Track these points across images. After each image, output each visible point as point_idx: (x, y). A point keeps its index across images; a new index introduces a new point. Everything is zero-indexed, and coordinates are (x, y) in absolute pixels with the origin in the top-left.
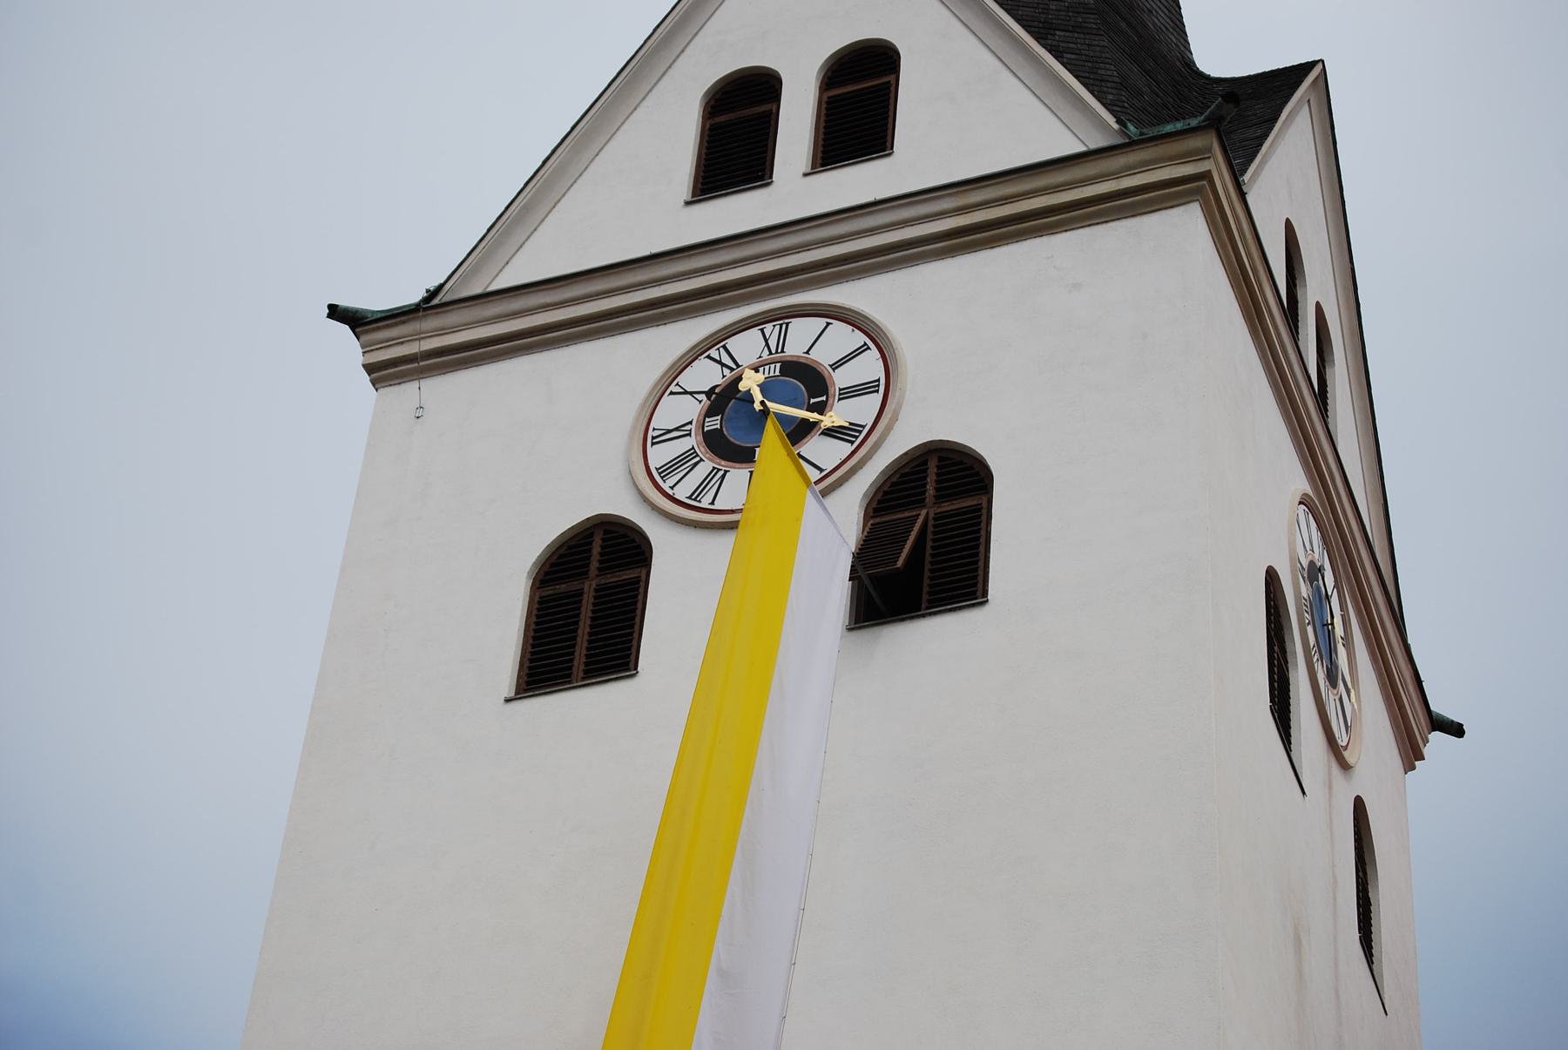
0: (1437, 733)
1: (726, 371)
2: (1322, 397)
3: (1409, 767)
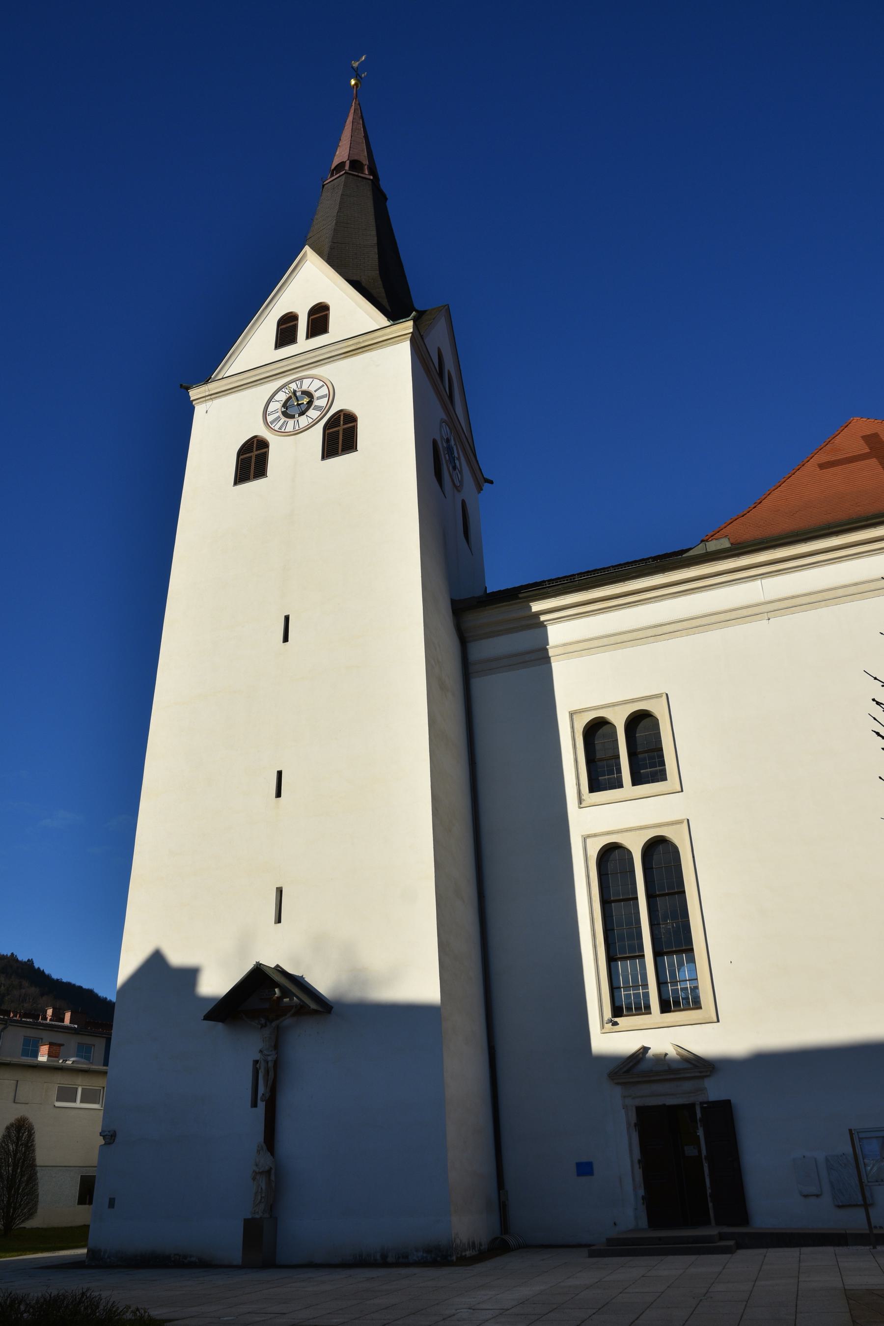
0: (486, 483)
1: (287, 394)
2: (451, 397)
3: (479, 492)
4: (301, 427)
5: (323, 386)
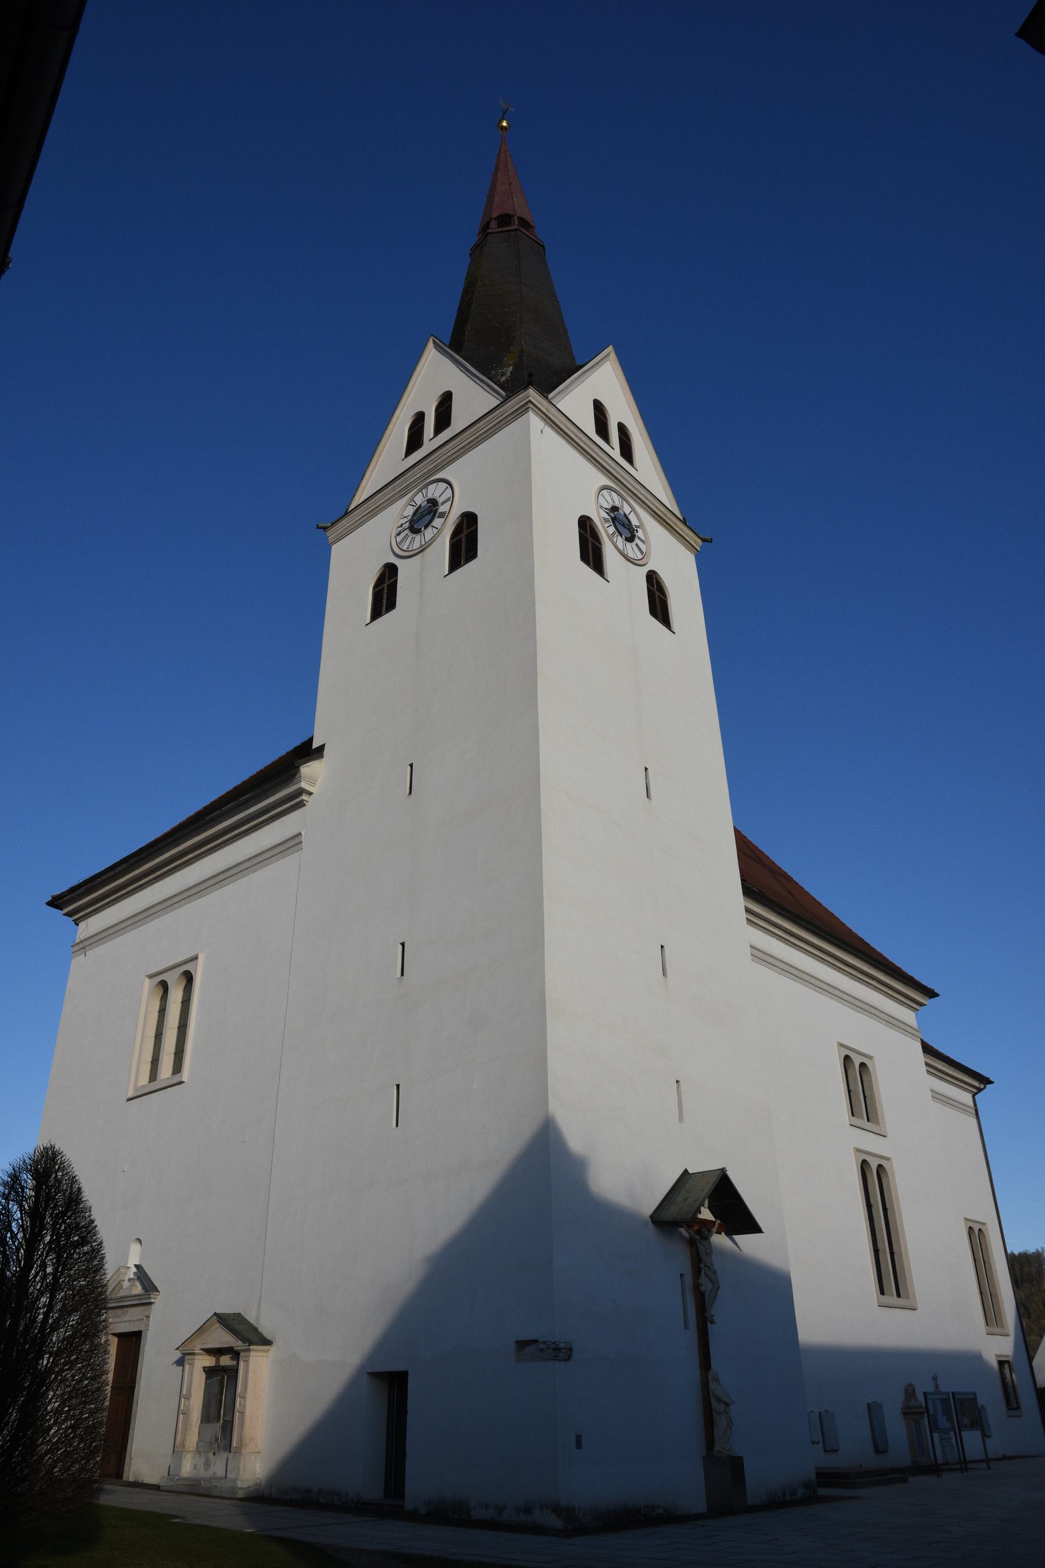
4: (427, 541)
5: (447, 487)
